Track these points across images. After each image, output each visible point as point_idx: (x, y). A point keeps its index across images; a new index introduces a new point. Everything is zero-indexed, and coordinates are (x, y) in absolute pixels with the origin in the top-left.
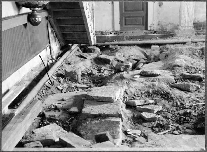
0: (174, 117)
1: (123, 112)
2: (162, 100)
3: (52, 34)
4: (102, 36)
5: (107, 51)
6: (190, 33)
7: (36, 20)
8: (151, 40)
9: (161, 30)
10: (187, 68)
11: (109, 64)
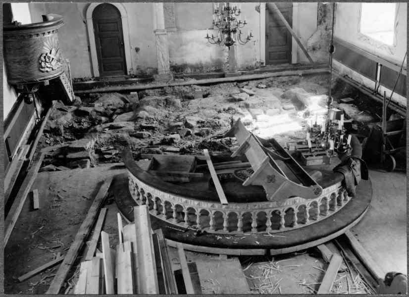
9: (141, 74)
11: (88, 115)
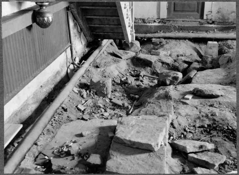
2: (226, 142)
3: (75, 28)
4: (144, 24)
7: (44, 20)
8: (207, 33)
9: (222, 19)
11: (150, 67)
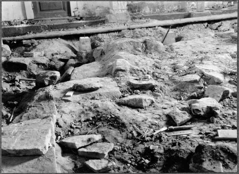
0: (132, 158)
1: (59, 165)
2: (111, 130)
4: (11, 27)
5: (21, 48)
6: (124, 18)
8: (78, 29)
9: (89, 15)
10: (133, 72)
11: (25, 69)
